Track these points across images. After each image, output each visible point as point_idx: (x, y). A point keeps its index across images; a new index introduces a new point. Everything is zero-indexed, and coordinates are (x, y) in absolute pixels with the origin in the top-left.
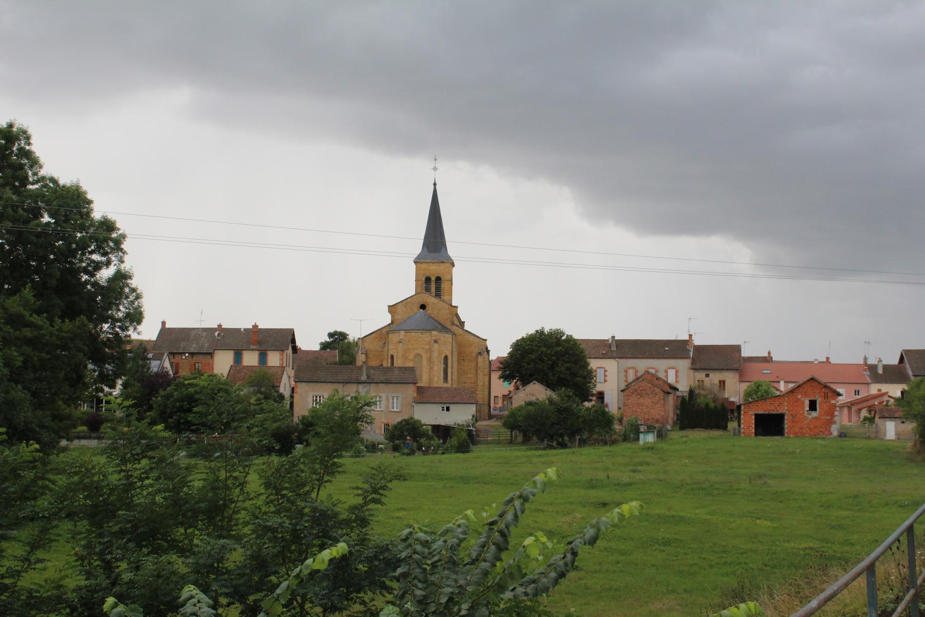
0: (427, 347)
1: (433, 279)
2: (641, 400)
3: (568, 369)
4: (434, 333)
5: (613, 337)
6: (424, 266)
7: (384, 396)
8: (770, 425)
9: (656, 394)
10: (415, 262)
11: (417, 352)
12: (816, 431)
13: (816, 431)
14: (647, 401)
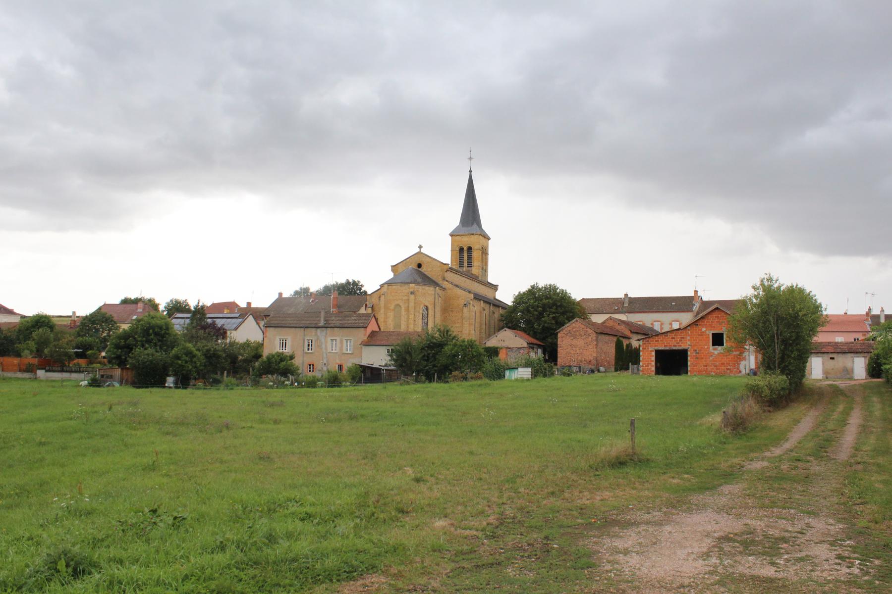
0: (406, 298)
1: (465, 248)
2: (575, 342)
3: (554, 318)
4: (412, 285)
5: (626, 295)
6: (458, 238)
7: (338, 339)
8: (672, 362)
9: (589, 335)
10: (451, 235)
11: (397, 303)
12: (724, 368)
13: (724, 368)
14: (580, 342)
